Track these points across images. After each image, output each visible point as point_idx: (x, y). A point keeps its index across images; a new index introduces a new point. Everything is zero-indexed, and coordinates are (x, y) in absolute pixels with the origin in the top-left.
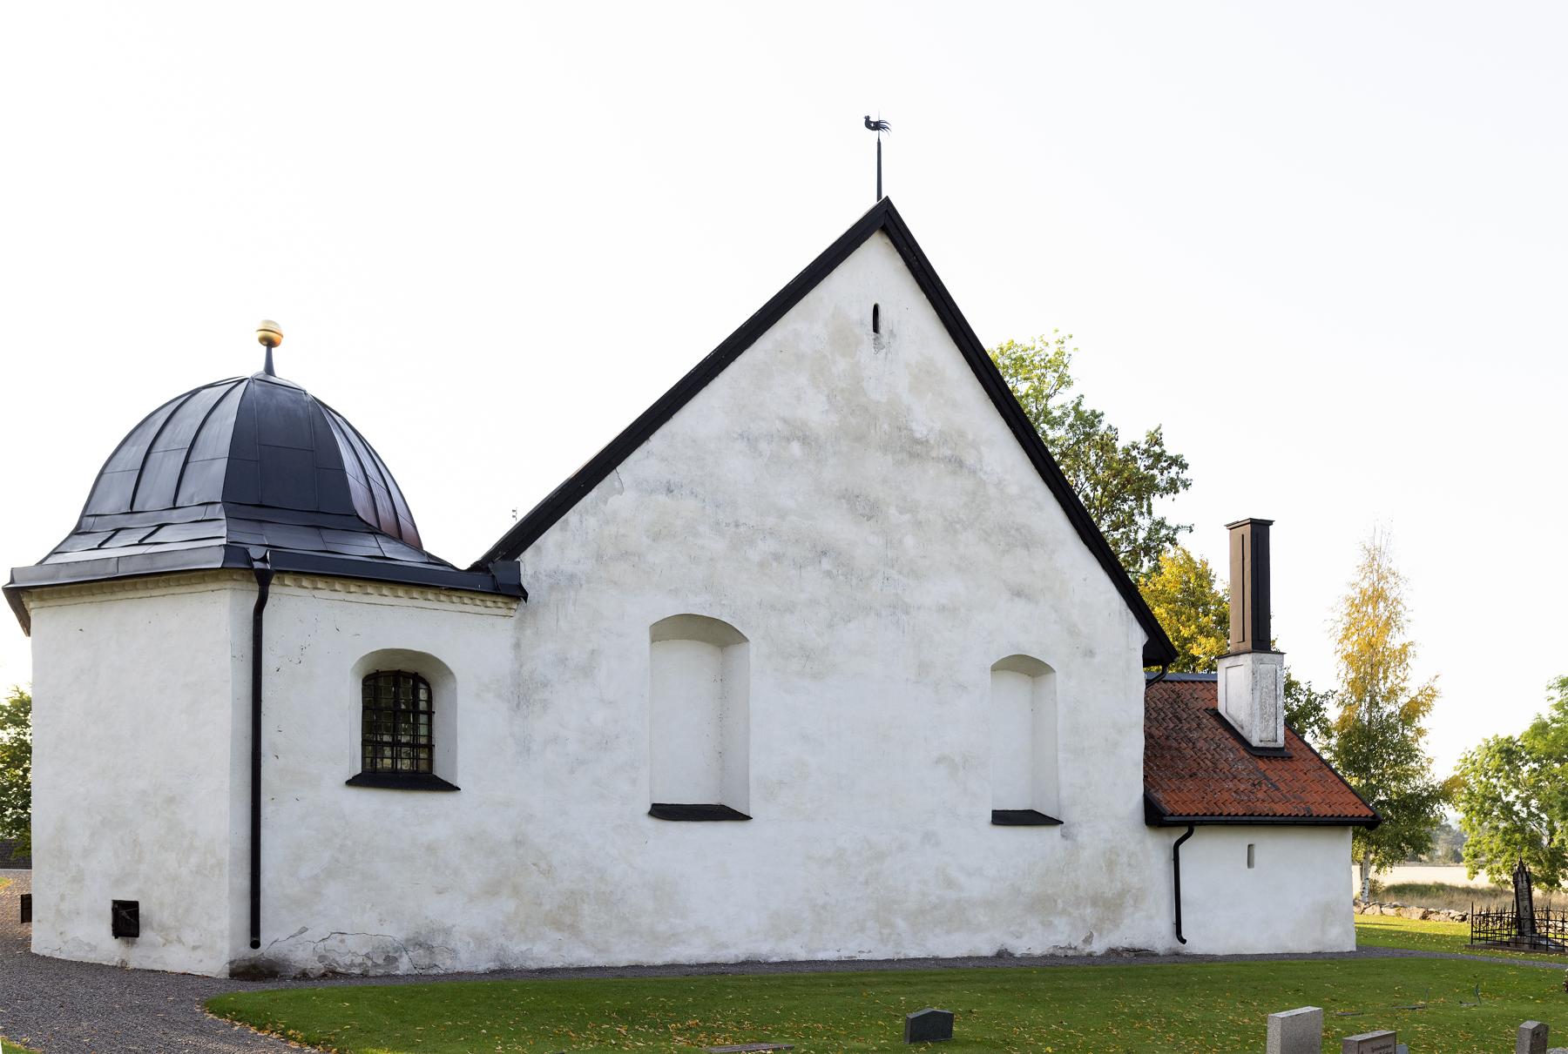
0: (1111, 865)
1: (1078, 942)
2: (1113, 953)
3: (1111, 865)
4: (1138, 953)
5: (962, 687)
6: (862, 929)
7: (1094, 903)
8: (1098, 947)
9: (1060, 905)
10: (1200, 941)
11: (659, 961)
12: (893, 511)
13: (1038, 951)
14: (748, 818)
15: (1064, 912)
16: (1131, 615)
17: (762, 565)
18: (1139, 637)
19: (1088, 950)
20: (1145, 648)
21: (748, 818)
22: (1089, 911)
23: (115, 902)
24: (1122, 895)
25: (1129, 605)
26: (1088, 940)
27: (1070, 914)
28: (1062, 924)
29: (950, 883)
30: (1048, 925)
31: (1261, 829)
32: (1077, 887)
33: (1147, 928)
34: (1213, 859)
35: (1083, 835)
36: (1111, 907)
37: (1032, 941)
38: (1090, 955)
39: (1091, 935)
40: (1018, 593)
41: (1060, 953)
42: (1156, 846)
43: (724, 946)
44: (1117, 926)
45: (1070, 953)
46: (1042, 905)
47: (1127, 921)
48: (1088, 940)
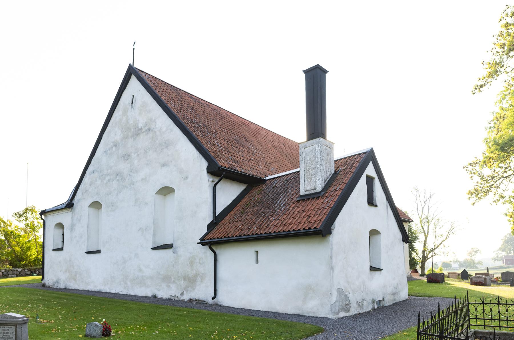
0: (192, 263)
1: (178, 295)
2: (191, 300)
3: (192, 263)
4: (198, 301)
5: (146, 204)
6: (120, 284)
7: (185, 280)
8: (186, 297)
9: (173, 280)
10: (226, 299)
11: (86, 289)
12: (133, 154)
13: (165, 297)
14: (380, 270)
15: (174, 282)
16: (201, 157)
17: (106, 184)
18: (205, 164)
19: (182, 298)
20: (208, 168)
21: (380, 270)
22: (183, 282)
23: (306, 72)
24: (196, 276)
25: (200, 153)
26: (182, 294)
27: (176, 283)
28: (173, 286)
29: (140, 270)
30: (169, 287)
31: (236, 244)
32: (178, 272)
33: (203, 292)
34: (236, 260)
35: (181, 251)
36: (192, 281)
37: (164, 293)
38: (183, 301)
39: (183, 293)
40: (164, 165)
41: (173, 298)
42: (206, 253)
43: (96, 287)
44: (194, 289)
45: (176, 299)
46: (167, 279)
47: (197, 287)
48: (182, 294)
